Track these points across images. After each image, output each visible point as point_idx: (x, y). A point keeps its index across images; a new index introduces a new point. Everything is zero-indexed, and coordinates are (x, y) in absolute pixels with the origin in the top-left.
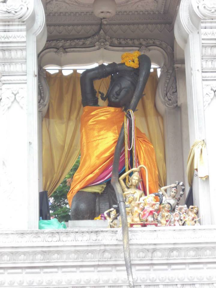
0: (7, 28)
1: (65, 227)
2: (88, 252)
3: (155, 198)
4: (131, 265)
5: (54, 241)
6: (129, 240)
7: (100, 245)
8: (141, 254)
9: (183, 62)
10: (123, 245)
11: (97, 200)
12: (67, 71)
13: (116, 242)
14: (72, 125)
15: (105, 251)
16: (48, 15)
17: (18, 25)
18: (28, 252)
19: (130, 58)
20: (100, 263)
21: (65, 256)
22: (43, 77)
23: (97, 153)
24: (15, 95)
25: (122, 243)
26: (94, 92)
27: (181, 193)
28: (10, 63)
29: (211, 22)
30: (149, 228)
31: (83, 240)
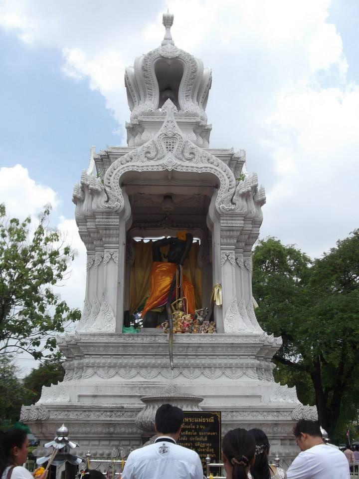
0: (108, 217)
1: (138, 332)
2: (150, 347)
3: (191, 316)
4: (173, 355)
5: (130, 340)
6: (172, 340)
7: (156, 343)
8: (181, 349)
9: (211, 237)
10: (169, 343)
11: (159, 316)
12: (146, 241)
13: (166, 342)
14: (148, 272)
15: (159, 347)
16: (133, 208)
17: (115, 215)
18: (115, 346)
19: (181, 235)
20: (157, 353)
21: (136, 349)
22: (130, 244)
23: (159, 289)
24: (112, 255)
25: (168, 342)
26: (160, 253)
27: (207, 314)
28: (110, 237)
29: (227, 217)
30: (185, 334)
31: (147, 340)
